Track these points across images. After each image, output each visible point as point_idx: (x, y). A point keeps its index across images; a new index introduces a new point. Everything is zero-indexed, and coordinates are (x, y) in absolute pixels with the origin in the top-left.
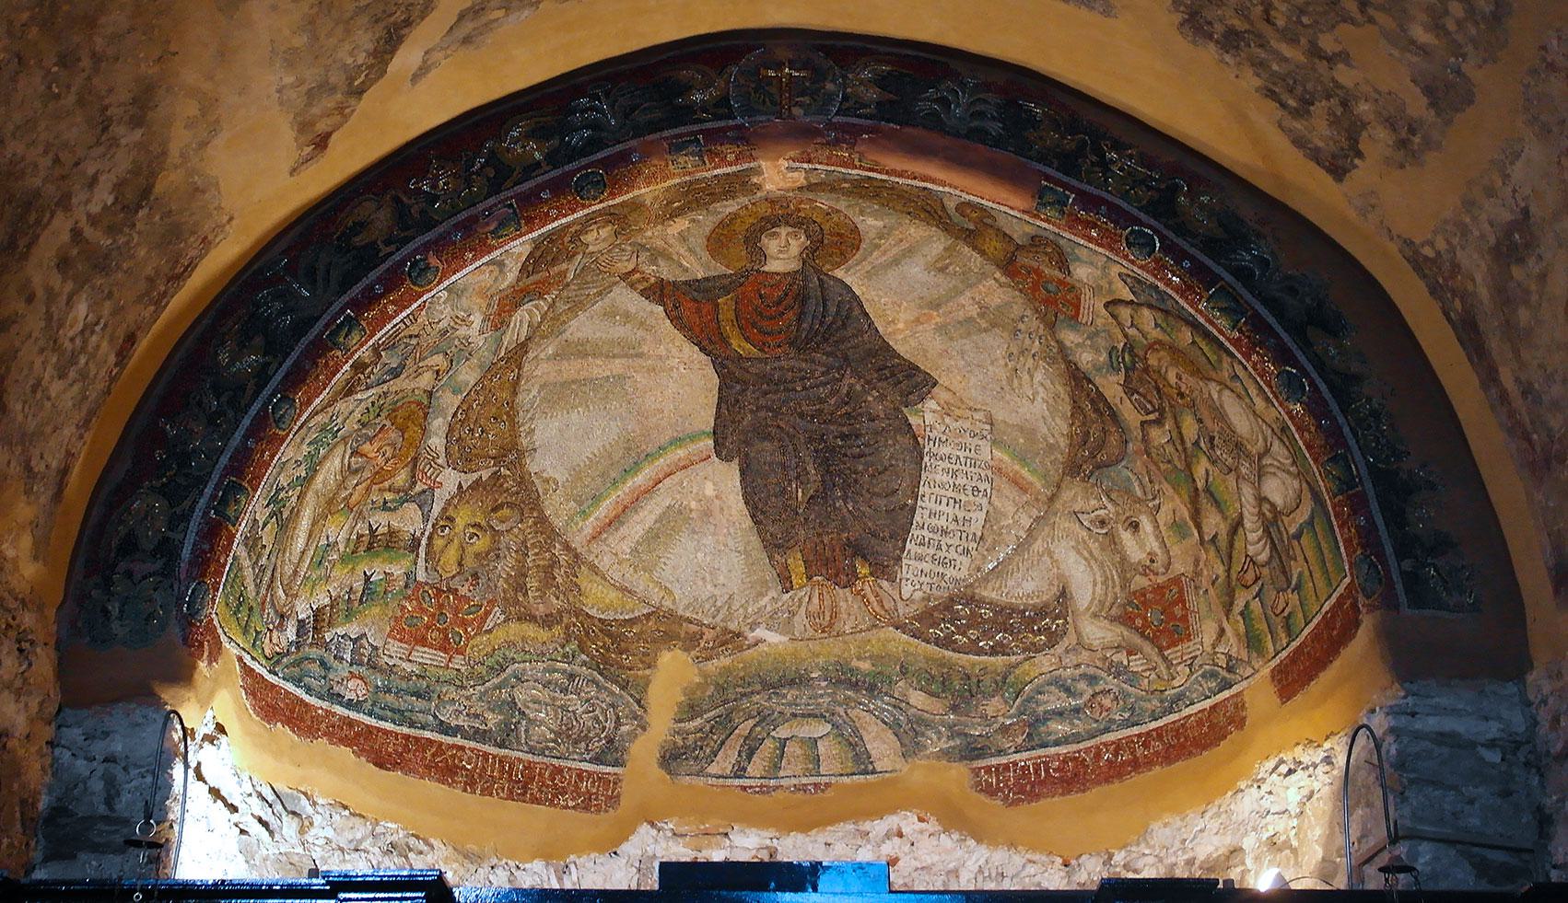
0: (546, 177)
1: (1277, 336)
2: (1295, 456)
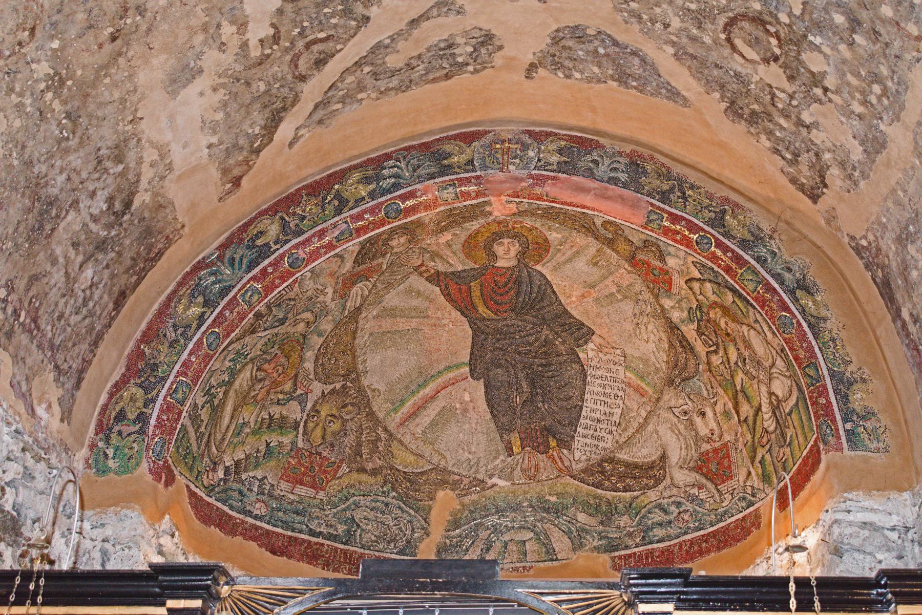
0: (367, 205)
2: (789, 365)
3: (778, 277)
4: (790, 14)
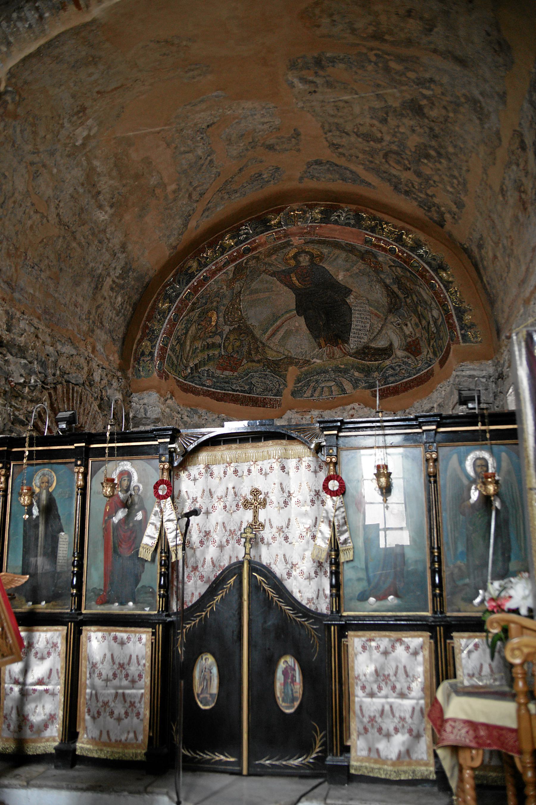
3: (429, 264)
4: (411, 151)
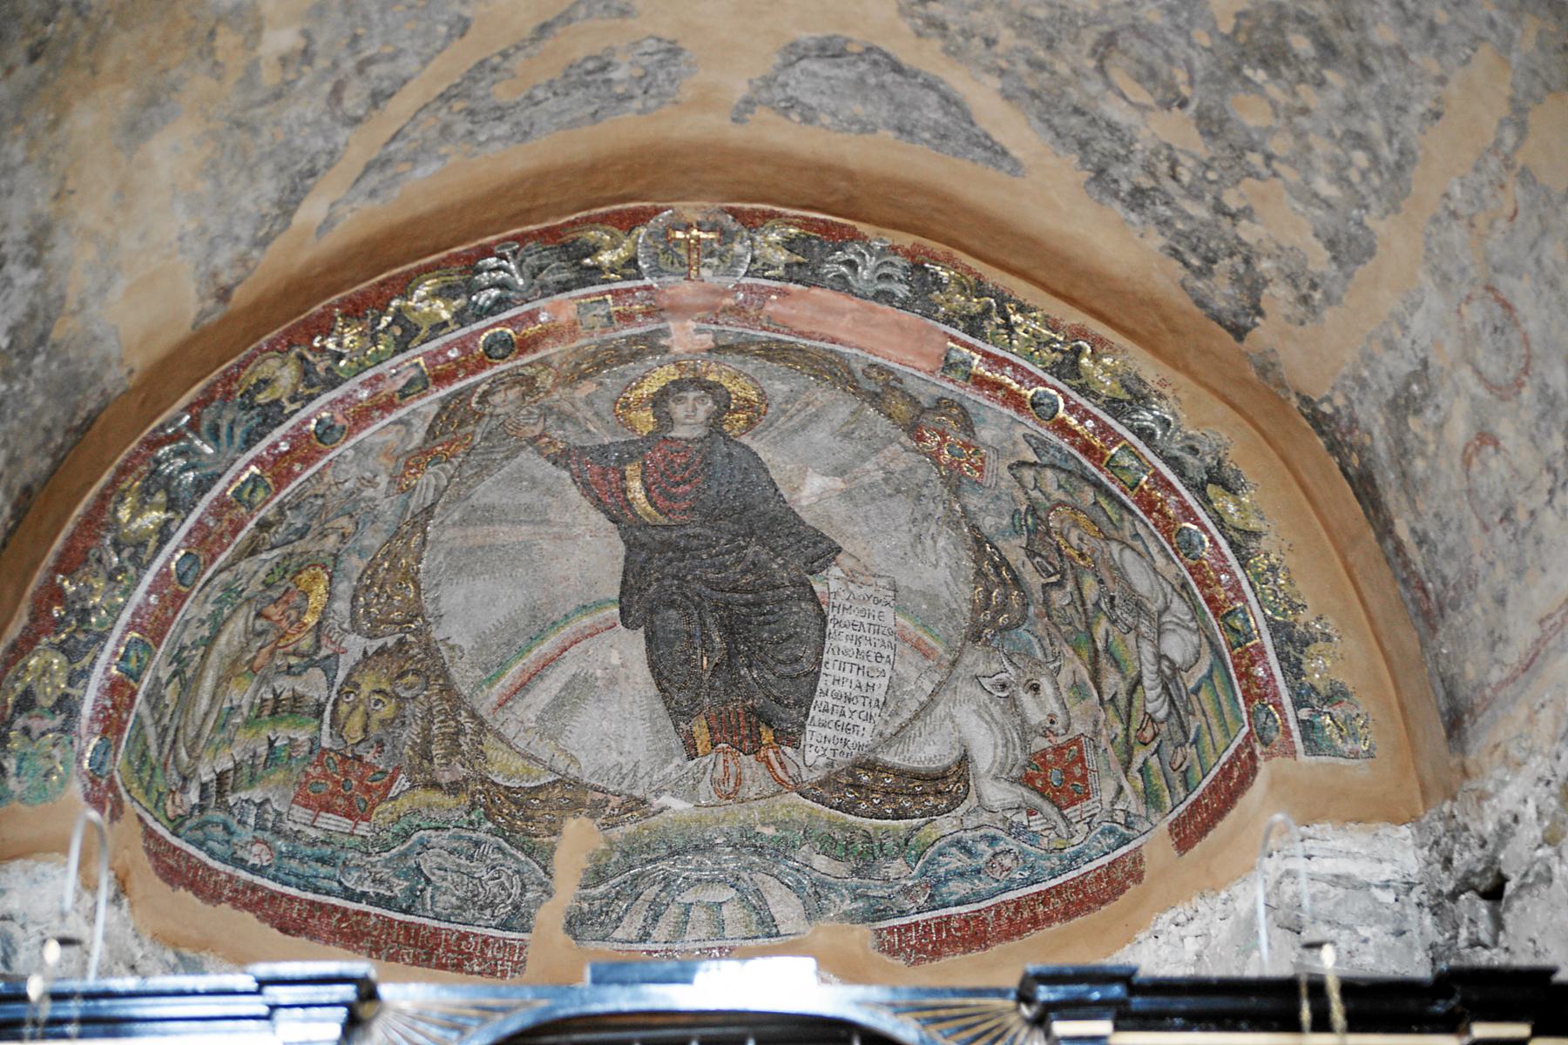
1: (1178, 494)
2: (1195, 609)
4: (1213, 31)
